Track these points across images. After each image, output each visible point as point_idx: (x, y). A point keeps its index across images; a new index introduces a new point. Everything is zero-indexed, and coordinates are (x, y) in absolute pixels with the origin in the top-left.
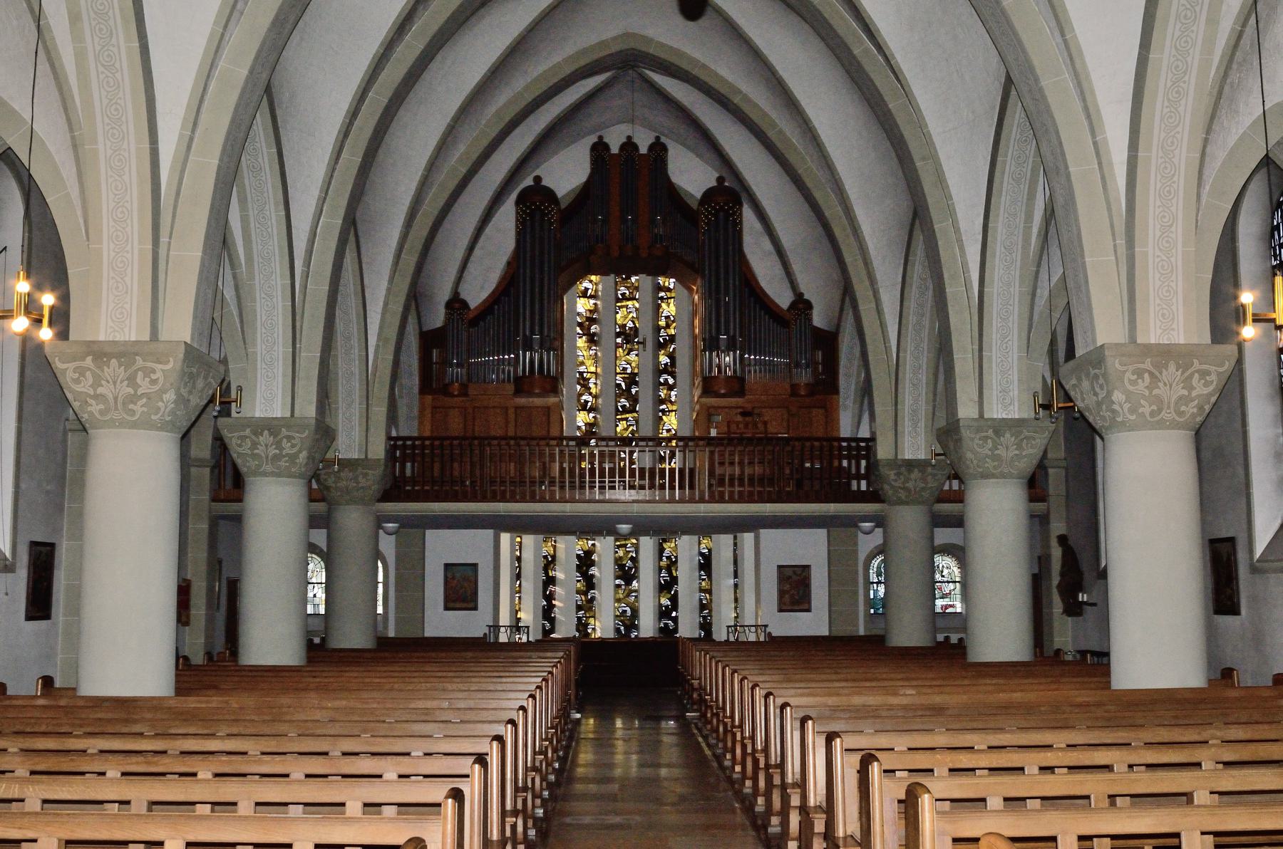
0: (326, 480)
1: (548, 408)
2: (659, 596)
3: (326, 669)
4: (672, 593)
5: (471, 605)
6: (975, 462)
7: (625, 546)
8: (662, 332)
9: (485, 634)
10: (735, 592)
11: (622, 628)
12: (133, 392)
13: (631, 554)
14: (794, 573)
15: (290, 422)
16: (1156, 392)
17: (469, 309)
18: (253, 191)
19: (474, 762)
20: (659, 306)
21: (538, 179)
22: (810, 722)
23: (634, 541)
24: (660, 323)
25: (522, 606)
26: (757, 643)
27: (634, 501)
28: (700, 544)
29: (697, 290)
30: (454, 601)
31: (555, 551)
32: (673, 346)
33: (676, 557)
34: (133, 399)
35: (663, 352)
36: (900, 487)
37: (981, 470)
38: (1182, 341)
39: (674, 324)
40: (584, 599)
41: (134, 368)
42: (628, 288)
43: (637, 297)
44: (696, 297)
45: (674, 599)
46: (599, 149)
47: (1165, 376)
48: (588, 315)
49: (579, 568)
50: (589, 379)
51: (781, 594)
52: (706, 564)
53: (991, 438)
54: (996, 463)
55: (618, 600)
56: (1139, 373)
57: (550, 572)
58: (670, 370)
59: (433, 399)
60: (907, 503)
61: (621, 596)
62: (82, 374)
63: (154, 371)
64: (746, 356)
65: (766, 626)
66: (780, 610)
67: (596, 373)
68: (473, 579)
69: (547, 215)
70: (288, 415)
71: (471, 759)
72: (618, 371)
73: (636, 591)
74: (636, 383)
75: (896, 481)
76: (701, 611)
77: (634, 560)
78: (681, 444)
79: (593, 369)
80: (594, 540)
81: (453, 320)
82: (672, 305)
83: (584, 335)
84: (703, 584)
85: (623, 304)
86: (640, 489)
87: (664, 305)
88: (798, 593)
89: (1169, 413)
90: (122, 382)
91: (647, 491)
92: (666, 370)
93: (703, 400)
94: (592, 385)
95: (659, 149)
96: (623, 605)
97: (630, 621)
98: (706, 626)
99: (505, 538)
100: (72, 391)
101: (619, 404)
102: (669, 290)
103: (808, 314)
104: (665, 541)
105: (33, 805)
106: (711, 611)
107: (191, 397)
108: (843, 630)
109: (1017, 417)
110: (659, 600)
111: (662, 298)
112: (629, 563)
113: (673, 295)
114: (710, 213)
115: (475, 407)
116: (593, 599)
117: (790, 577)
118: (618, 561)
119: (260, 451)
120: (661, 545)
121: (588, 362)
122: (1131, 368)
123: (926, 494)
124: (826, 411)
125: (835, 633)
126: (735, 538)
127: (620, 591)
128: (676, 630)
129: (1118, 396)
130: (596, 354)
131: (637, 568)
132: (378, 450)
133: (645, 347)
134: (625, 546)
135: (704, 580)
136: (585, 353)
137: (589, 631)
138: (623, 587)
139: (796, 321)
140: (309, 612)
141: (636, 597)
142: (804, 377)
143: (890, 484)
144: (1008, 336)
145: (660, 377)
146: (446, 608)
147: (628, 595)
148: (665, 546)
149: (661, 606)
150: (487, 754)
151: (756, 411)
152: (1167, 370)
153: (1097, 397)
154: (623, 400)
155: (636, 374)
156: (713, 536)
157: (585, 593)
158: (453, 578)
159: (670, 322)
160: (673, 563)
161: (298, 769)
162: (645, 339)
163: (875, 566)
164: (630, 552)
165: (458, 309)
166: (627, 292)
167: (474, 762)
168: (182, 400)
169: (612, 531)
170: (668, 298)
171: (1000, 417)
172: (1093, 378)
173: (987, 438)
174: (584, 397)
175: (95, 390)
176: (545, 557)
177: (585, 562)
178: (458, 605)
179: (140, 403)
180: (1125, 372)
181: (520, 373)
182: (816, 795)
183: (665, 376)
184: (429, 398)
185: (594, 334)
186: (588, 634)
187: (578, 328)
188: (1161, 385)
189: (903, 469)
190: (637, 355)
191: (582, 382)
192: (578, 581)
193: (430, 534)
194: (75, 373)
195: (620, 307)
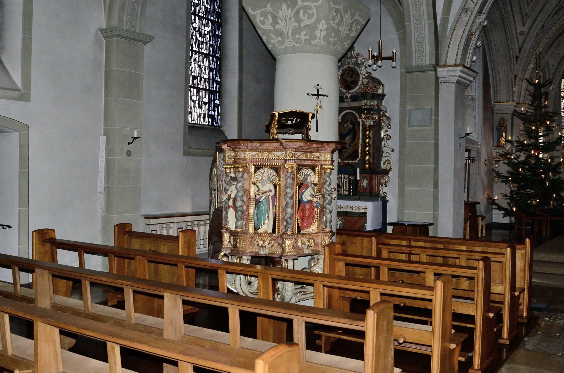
16: (277, 26)
34: (297, 31)
47: (281, 14)
62: (266, 17)
63: (310, 8)
89: (290, 41)
100: (261, 29)
107: (340, 28)
179: (303, 33)
188: (279, 21)
194: (261, 17)
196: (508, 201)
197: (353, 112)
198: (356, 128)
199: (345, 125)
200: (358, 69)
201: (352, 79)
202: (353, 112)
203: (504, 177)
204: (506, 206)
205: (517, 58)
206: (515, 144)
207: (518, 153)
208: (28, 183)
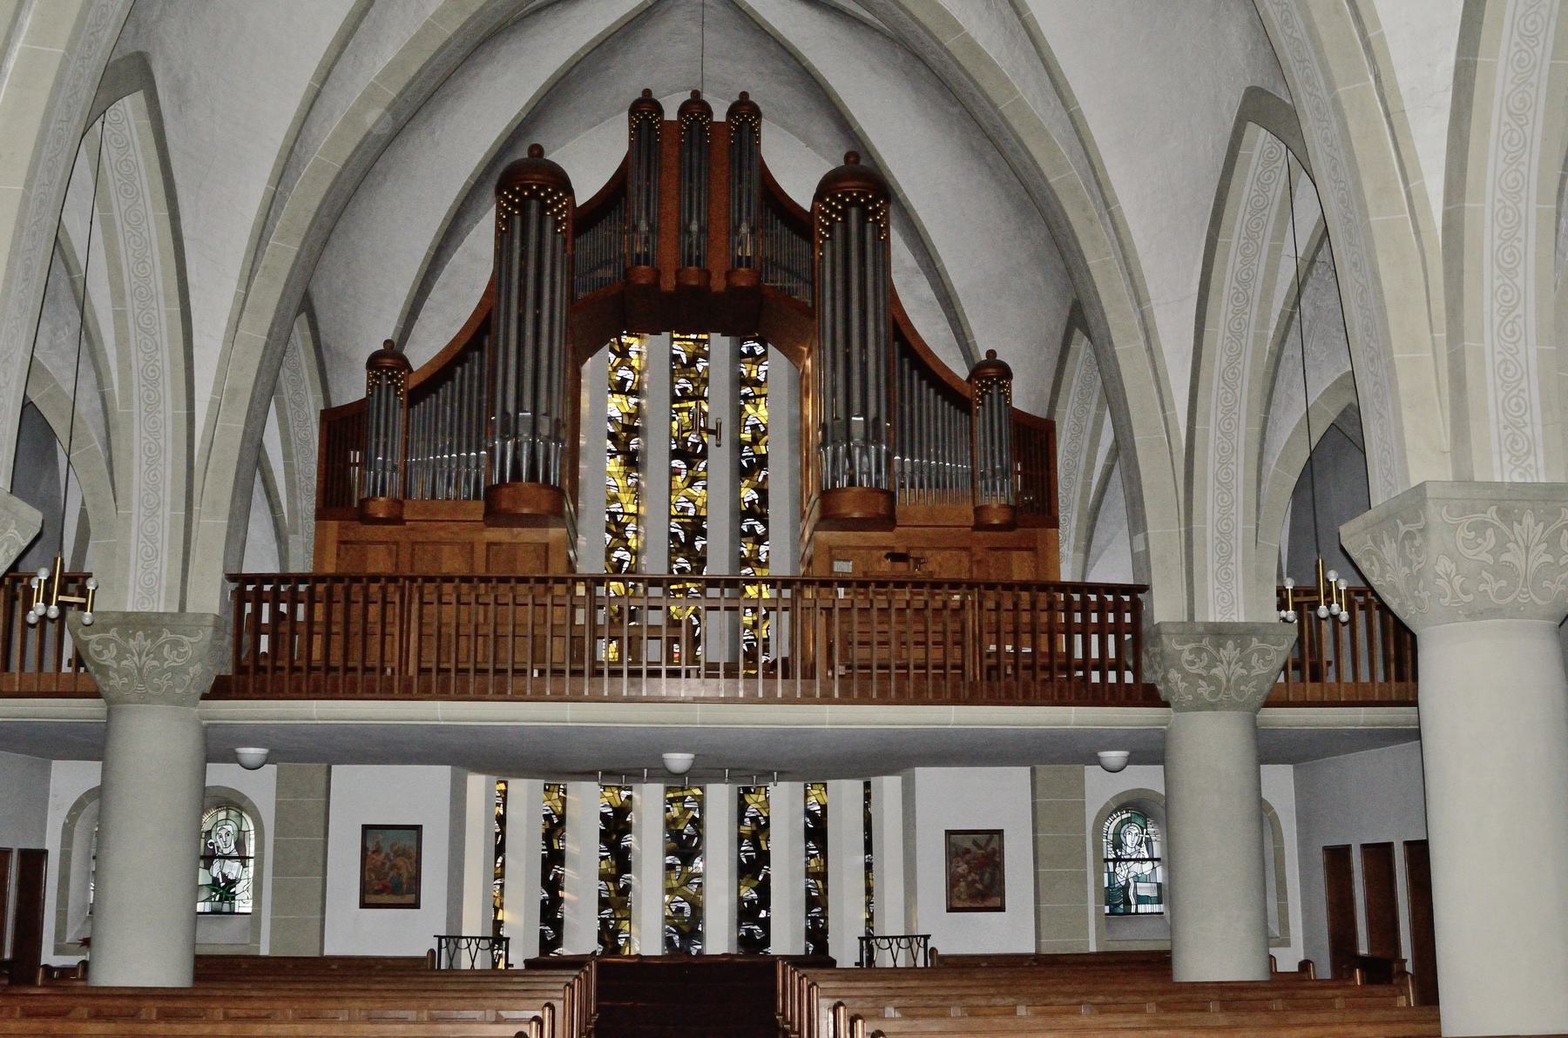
0: (99, 653)
1: (547, 546)
2: (739, 884)
3: (254, 993)
4: (761, 878)
5: (410, 898)
6: (1457, 581)
7: (682, 799)
8: (746, 452)
9: (432, 951)
10: (867, 878)
11: (676, 938)
13: (691, 813)
14: (975, 843)
15: (178, 620)
17: (411, 371)
18: (134, 280)
20: (742, 409)
21: (537, 151)
23: (698, 792)
24: (742, 436)
25: (506, 901)
26: (911, 971)
27: (696, 700)
28: (806, 796)
29: (810, 351)
30: (377, 892)
31: (564, 808)
32: (763, 473)
33: (767, 819)
35: (747, 482)
36: (1201, 676)
37: (1468, 598)
38: (1242, 620)
39: (765, 438)
40: (612, 888)
42: (690, 380)
43: (706, 394)
44: (809, 362)
45: (764, 889)
46: (644, 109)
48: (626, 422)
49: (604, 836)
50: (626, 524)
51: (952, 882)
52: (817, 831)
53: (1493, 525)
54: (1504, 583)
55: (670, 891)
57: (555, 841)
58: (758, 513)
59: (340, 527)
60: (1213, 707)
61: (675, 884)
64: (897, 458)
65: (927, 937)
66: (951, 909)
67: (636, 515)
68: (413, 852)
69: (550, 207)
70: (175, 609)
72: (674, 512)
73: (699, 875)
74: (703, 533)
75: (1192, 663)
76: (808, 909)
77: (697, 823)
78: (787, 593)
79: (632, 509)
80: (630, 789)
81: (380, 385)
82: (762, 407)
83: (618, 452)
84: (813, 863)
85: (683, 405)
86: (707, 676)
87: (749, 408)
88: (982, 879)
91: (722, 681)
92: (751, 512)
93: (822, 535)
94: (630, 535)
95: (746, 112)
96: (678, 898)
97: (686, 926)
98: (817, 934)
99: (477, 785)
101: (677, 386)
102: (757, 383)
103: (1003, 386)
104: (747, 790)
106: (825, 909)
108: (1056, 944)
109: (1543, 480)
110: (739, 890)
111: (746, 398)
112: (689, 829)
113: (764, 391)
114: (834, 209)
115: (414, 543)
116: (628, 888)
117: (968, 851)
118: (670, 824)
120: (741, 797)
121: (624, 498)
123: (1247, 690)
124: (1036, 555)
125: (1045, 951)
126: (867, 785)
127: (673, 876)
128: (766, 942)
130: (637, 484)
131: (700, 836)
132: (209, 597)
133: (719, 438)
134: (682, 799)
135: (813, 856)
136: (620, 483)
137: (621, 943)
138: (678, 869)
139: (982, 397)
140: (198, 910)
141: (700, 885)
142: (997, 500)
143: (1180, 670)
144: (1515, 307)
145: (742, 522)
146: (364, 905)
147: (687, 882)
148: (748, 799)
149: (740, 900)
151: (913, 554)
153: (1410, 567)
154: (680, 560)
155: (704, 518)
156: (829, 783)
157: (615, 879)
158: (377, 851)
159: (758, 435)
160: (761, 829)
162: (719, 425)
163: (1111, 831)
164: (690, 809)
165: (390, 369)
166: (690, 387)
169: (660, 773)
170: (756, 397)
171: (1507, 480)
172: (1404, 539)
173: (1485, 525)
174: (617, 554)
175: (119, 663)
176: (548, 817)
177: (615, 826)
178: (385, 899)
181: (496, 480)
183: (750, 521)
184: (333, 525)
185: (635, 452)
186: (619, 948)
187: (609, 442)
189: (1206, 642)
190: (705, 487)
191: (613, 528)
192: (603, 858)
193: (342, 774)
195: (679, 410)
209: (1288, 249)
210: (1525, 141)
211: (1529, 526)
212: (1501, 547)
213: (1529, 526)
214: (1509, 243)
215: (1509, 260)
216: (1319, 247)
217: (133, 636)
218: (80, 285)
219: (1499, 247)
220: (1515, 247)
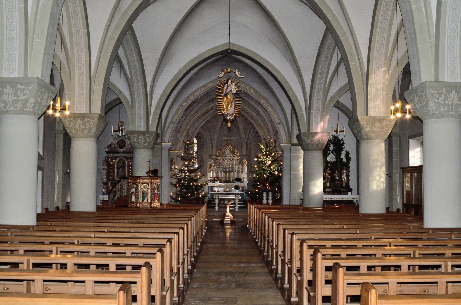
12: (16, 98)
19: (167, 242)
22: (286, 230)
41: (16, 89)
56: (440, 94)
63: (150, 137)
71: (166, 240)
90: (11, 94)
100: (67, 127)
105: (21, 252)
119: (77, 127)
122: (436, 92)
129: (431, 104)
150: (173, 239)
152: (451, 93)
161: (93, 250)
167: (167, 242)
168: (97, 129)
179: (147, 144)
180: (434, 94)
182: (307, 275)
196: (176, 195)
197: (123, 158)
198: (125, 165)
199: (120, 164)
200: (125, 140)
201: (123, 144)
202: (123, 158)
203: (174, 185)
204: (175, 198)
205: (179, 131)
206: (179, 170)
207: (181, 174)
208: (290, 195)
209: (395, 22)
210: (455, 57)
211: (454, 95)
212: (446, 99)
213: (454, 95)
214: (452, 44)
215: (452, 49)
216: (401, 26)
217: (77, 120)
218: (61, 30)
219: (452, 3)
220: (457, 3)
